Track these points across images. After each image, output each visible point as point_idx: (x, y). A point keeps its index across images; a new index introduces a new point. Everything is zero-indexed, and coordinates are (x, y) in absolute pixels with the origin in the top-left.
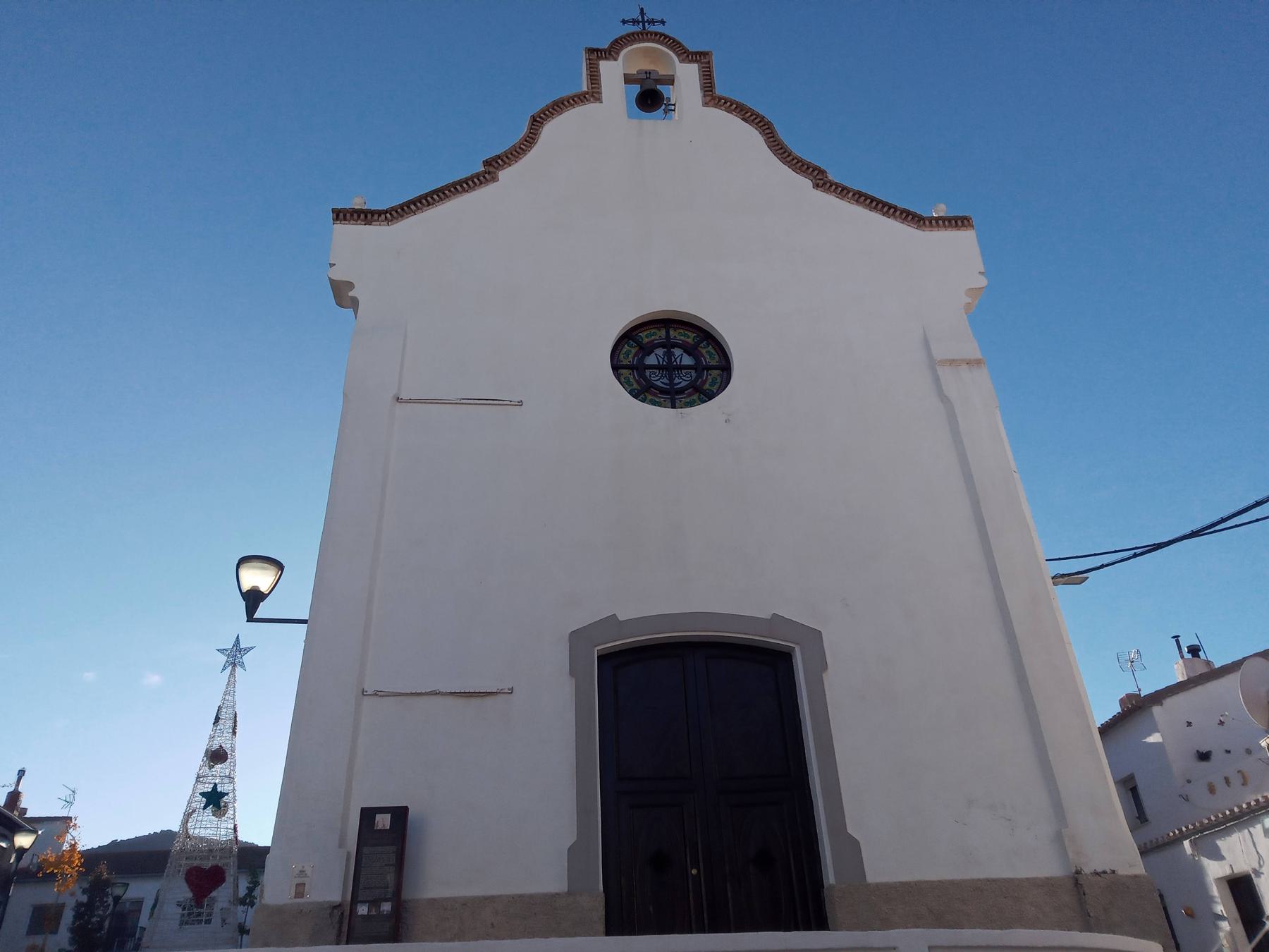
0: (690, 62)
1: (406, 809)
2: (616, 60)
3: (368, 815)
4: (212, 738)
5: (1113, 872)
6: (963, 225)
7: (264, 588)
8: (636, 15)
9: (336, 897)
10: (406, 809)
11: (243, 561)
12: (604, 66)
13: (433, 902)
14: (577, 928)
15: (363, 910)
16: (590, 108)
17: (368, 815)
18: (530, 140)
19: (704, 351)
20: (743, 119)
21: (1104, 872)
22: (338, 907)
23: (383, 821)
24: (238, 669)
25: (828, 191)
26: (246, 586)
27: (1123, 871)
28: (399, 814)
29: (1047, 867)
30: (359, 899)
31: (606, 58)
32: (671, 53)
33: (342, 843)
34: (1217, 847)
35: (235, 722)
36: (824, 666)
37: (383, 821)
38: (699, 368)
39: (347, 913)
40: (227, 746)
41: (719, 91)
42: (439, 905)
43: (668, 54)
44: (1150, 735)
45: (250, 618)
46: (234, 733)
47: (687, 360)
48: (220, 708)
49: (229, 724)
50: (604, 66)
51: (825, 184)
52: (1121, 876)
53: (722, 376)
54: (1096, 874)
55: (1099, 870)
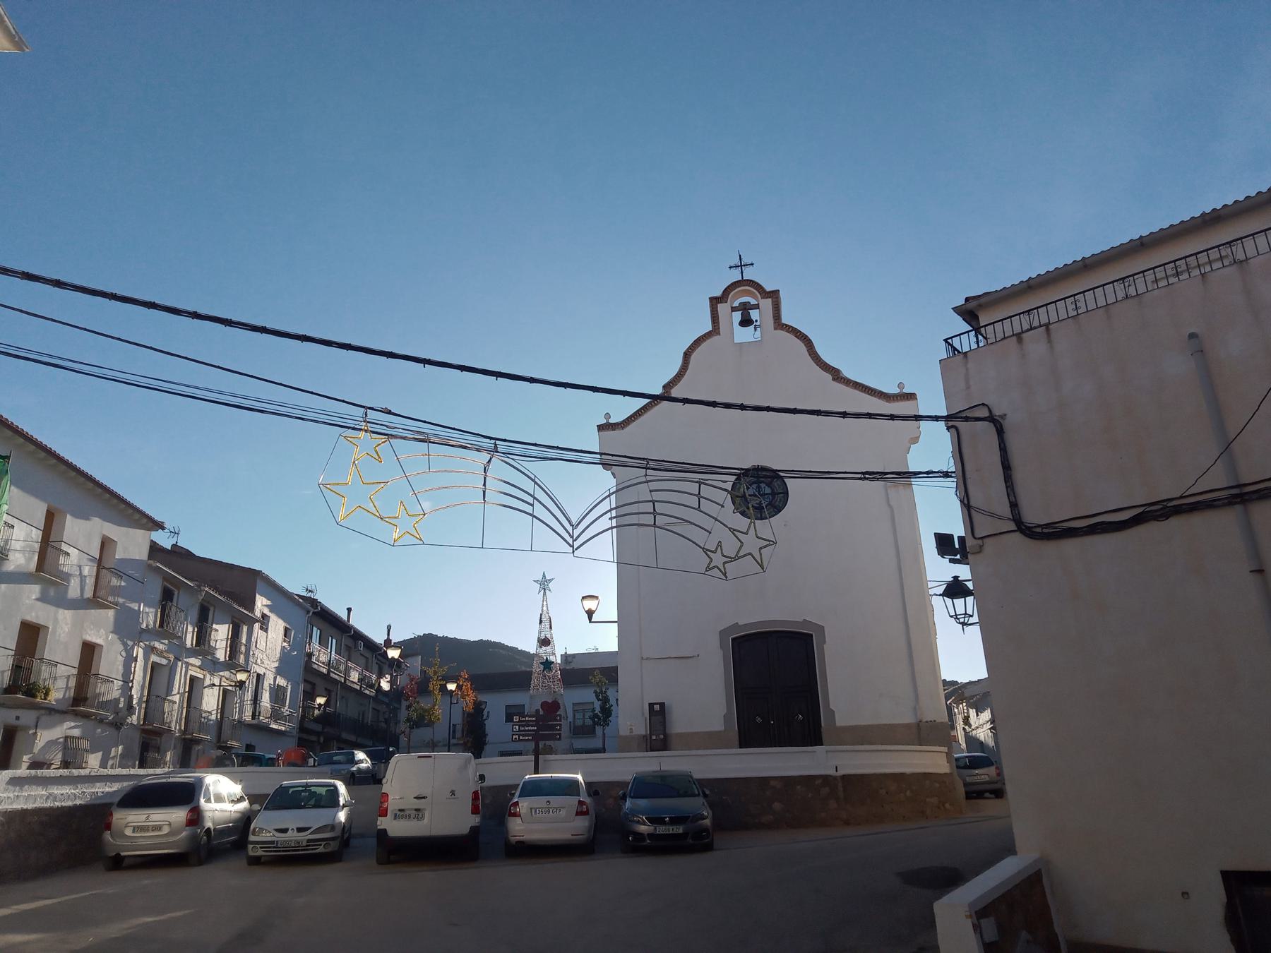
0: (767, 298)
1: (664, 703)
2: (727, 302)
3: (651, 705)
4: (540, 632)
5: (935, 721)
6: (911, 398)
7: (593, 609)
8: (737, 262)
9: (644, 733)
10: (664, 703)
11: (583, 598)
12: (720, 306)
13: (677, 734)
14: (727, 746)
15: (654, 737)
16: (715, 339)
17: (651, 705)
18: (687, 355)
19: (776, 484)
20: (796, 337)
21: (931, 721)
22: (645, 736)
23: (657, 708)
24: (547, 591)
25: (840, 382)
26: (586, 609)
27: (939, 720)
28: (662, 705)
29: (908, 719)
30: (929, 587)
31: (721, 302)
32: (755, 291)
33: (643, 714)
34: (985, 710)
35: (550, 621)
36: (825, 642)
37: (657, 708)
38: (773, 494)
39: (649, 738)
40: (549, 636)
41: (784, 320)
42: (681, 735)
43: (754, 293)
44: (339, 801)
45: (590, 622)
46: (551, 628)
47: (768, 490)
48: (541, 615)
49: (547, 624)
50: (720, 306)
51: (838, 378)
52: (938, 723)
53: (783, 497)
54: (927, 722)
55: (929, 720)
